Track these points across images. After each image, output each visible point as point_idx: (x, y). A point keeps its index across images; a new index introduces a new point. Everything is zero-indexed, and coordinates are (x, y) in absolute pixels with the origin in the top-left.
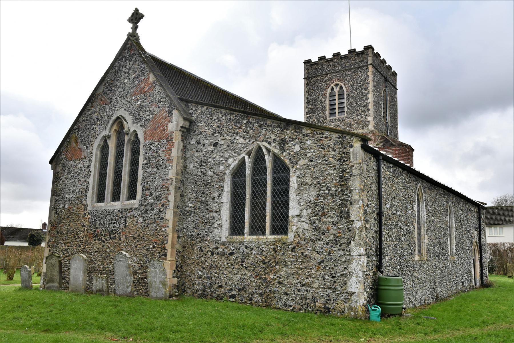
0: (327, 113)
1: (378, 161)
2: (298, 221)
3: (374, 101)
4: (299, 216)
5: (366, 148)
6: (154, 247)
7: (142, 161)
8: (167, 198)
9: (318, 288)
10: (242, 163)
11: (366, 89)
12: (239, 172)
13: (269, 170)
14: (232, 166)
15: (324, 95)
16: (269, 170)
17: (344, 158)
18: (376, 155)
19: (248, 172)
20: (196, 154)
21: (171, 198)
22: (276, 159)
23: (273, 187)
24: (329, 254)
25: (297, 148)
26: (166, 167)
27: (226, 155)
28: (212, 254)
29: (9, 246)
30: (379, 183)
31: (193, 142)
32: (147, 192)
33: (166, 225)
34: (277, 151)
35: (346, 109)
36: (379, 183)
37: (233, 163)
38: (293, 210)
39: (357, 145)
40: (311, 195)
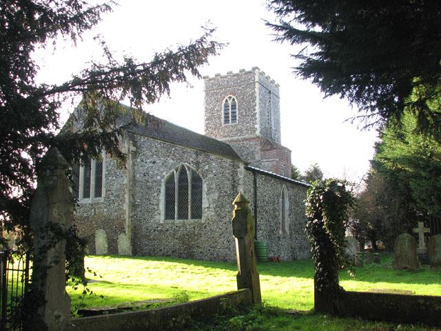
0: (223, 120)
1: (255, 175)
2: (208, 210)
3: (260, 112)
4: (209, 208)
5: (247, 169)
6: (116, 227)
7: (104, 172)
8: (124, 196)
9: (222, 252)
10: (173, 175)
11: (254, 101)
12: (170, 181)
13: (189, 180)
14: (166, 177)
15: (220, 105)
16: (189, 180)
17: (234, 174)
18: (254, 171)
19: (176, 181)
20: (141, 168)
21: (126, 196)
22: (193, 173)
23: (192, 191)
24: (226, 229)
25: (207, 167)
26: (122, 177)
27: (162, 170)
28: (154, 231)
29: (187, 253)
30: (255, 188)
31: (139, 160)
32: (109, 192)
33: (124, 213)
34: (194, 169)
35: (237, 118)
36: (255, 188)
37: (166, 175)
38: (205, 204)
39: (242, 166)
40: (216, 196)
